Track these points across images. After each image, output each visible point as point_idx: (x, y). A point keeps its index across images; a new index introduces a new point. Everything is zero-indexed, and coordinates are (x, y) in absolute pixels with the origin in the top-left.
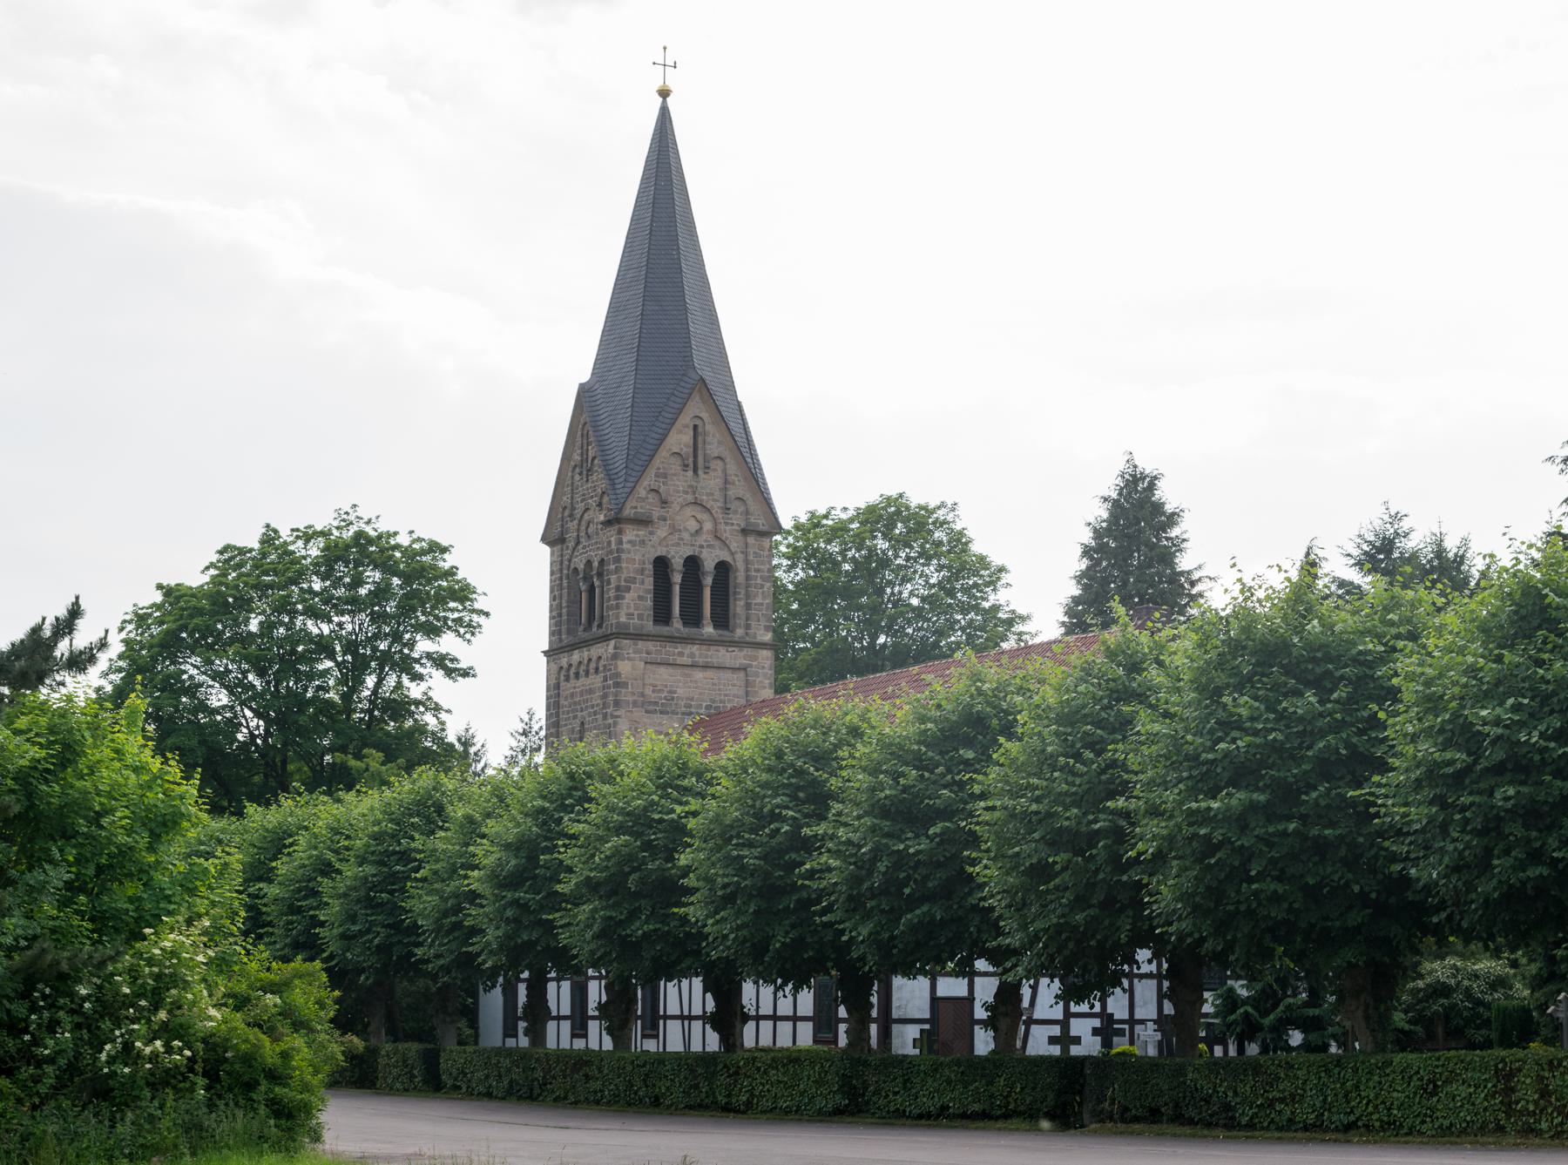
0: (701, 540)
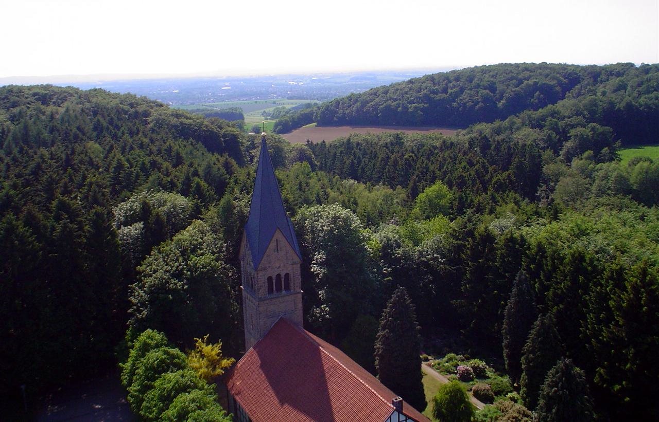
0: (280, 269)
